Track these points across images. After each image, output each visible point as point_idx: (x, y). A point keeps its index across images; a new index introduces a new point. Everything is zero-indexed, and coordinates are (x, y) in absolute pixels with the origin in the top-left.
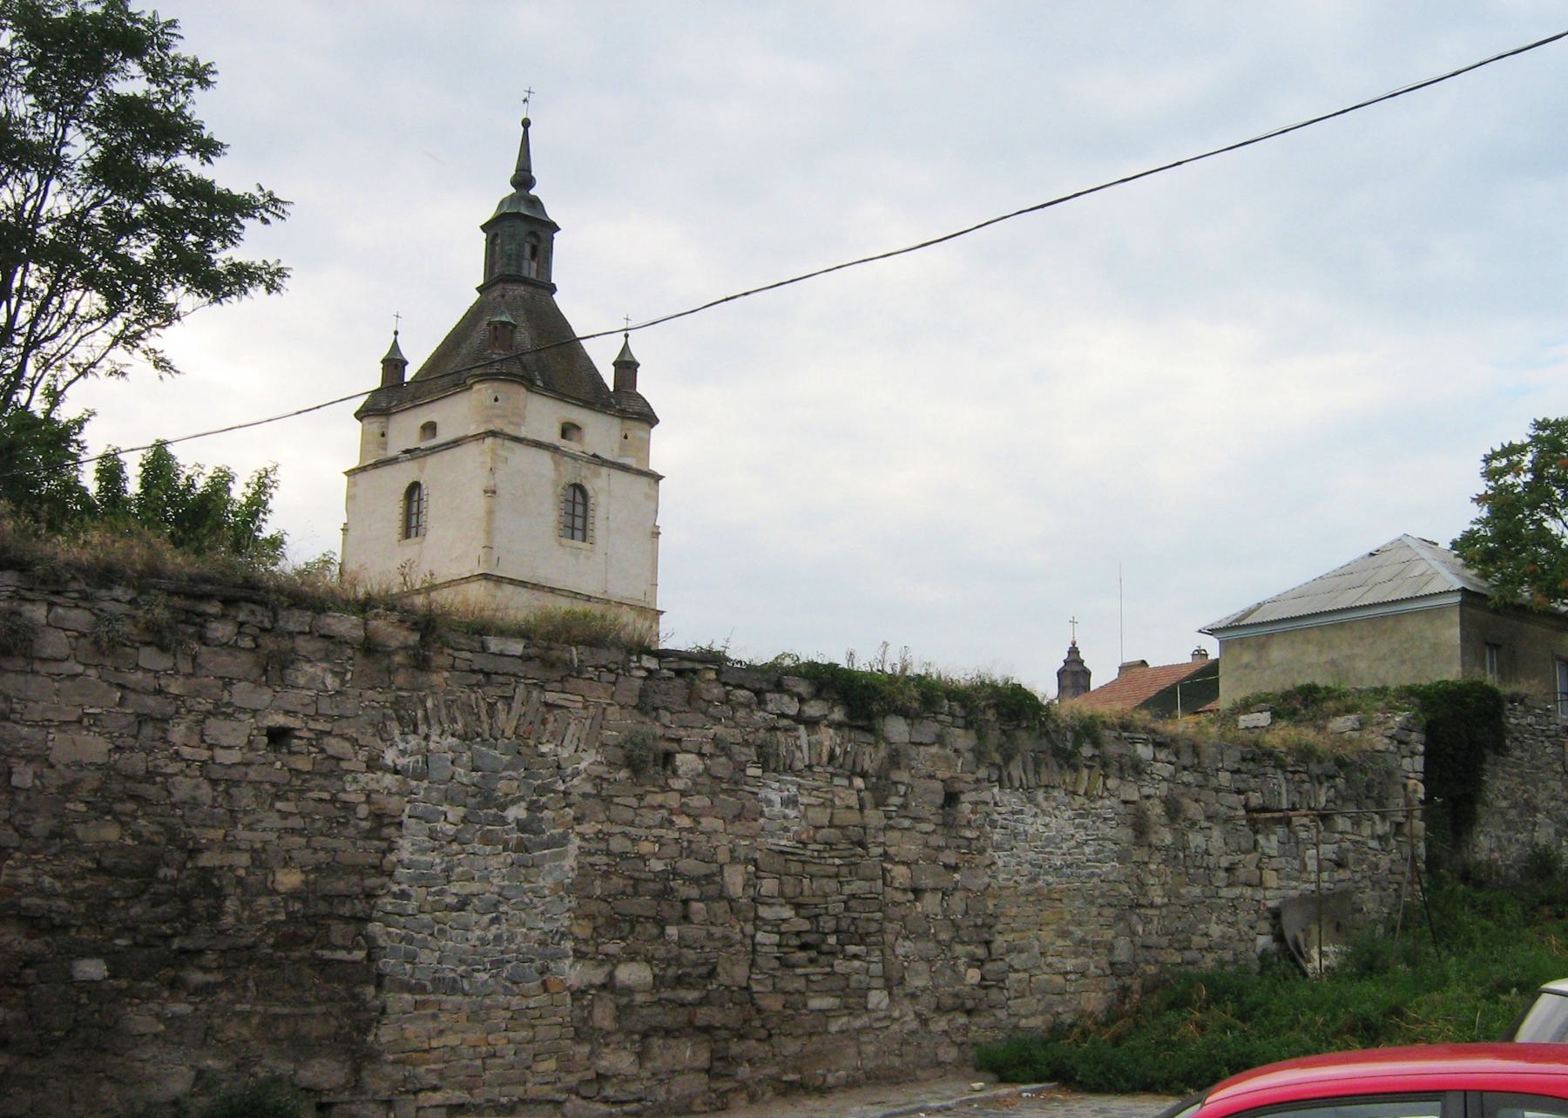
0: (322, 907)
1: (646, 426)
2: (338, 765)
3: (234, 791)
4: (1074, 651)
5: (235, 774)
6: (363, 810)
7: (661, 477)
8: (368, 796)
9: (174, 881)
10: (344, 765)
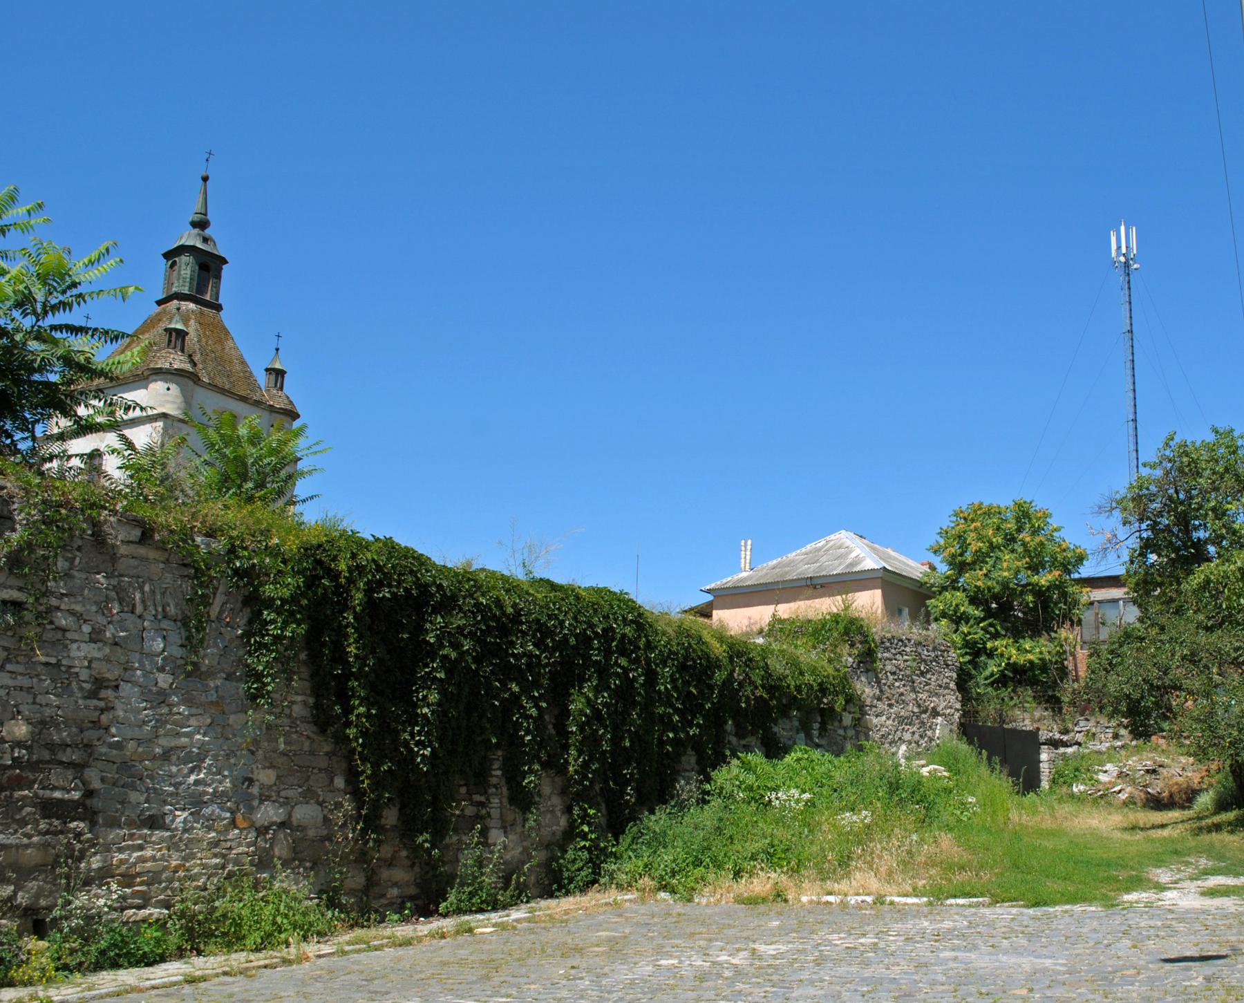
0: (46, 755)
1: (289, 419)
2: (64, 635)
6: (84, 675)
8: (90, 662)
10: (68, 635)
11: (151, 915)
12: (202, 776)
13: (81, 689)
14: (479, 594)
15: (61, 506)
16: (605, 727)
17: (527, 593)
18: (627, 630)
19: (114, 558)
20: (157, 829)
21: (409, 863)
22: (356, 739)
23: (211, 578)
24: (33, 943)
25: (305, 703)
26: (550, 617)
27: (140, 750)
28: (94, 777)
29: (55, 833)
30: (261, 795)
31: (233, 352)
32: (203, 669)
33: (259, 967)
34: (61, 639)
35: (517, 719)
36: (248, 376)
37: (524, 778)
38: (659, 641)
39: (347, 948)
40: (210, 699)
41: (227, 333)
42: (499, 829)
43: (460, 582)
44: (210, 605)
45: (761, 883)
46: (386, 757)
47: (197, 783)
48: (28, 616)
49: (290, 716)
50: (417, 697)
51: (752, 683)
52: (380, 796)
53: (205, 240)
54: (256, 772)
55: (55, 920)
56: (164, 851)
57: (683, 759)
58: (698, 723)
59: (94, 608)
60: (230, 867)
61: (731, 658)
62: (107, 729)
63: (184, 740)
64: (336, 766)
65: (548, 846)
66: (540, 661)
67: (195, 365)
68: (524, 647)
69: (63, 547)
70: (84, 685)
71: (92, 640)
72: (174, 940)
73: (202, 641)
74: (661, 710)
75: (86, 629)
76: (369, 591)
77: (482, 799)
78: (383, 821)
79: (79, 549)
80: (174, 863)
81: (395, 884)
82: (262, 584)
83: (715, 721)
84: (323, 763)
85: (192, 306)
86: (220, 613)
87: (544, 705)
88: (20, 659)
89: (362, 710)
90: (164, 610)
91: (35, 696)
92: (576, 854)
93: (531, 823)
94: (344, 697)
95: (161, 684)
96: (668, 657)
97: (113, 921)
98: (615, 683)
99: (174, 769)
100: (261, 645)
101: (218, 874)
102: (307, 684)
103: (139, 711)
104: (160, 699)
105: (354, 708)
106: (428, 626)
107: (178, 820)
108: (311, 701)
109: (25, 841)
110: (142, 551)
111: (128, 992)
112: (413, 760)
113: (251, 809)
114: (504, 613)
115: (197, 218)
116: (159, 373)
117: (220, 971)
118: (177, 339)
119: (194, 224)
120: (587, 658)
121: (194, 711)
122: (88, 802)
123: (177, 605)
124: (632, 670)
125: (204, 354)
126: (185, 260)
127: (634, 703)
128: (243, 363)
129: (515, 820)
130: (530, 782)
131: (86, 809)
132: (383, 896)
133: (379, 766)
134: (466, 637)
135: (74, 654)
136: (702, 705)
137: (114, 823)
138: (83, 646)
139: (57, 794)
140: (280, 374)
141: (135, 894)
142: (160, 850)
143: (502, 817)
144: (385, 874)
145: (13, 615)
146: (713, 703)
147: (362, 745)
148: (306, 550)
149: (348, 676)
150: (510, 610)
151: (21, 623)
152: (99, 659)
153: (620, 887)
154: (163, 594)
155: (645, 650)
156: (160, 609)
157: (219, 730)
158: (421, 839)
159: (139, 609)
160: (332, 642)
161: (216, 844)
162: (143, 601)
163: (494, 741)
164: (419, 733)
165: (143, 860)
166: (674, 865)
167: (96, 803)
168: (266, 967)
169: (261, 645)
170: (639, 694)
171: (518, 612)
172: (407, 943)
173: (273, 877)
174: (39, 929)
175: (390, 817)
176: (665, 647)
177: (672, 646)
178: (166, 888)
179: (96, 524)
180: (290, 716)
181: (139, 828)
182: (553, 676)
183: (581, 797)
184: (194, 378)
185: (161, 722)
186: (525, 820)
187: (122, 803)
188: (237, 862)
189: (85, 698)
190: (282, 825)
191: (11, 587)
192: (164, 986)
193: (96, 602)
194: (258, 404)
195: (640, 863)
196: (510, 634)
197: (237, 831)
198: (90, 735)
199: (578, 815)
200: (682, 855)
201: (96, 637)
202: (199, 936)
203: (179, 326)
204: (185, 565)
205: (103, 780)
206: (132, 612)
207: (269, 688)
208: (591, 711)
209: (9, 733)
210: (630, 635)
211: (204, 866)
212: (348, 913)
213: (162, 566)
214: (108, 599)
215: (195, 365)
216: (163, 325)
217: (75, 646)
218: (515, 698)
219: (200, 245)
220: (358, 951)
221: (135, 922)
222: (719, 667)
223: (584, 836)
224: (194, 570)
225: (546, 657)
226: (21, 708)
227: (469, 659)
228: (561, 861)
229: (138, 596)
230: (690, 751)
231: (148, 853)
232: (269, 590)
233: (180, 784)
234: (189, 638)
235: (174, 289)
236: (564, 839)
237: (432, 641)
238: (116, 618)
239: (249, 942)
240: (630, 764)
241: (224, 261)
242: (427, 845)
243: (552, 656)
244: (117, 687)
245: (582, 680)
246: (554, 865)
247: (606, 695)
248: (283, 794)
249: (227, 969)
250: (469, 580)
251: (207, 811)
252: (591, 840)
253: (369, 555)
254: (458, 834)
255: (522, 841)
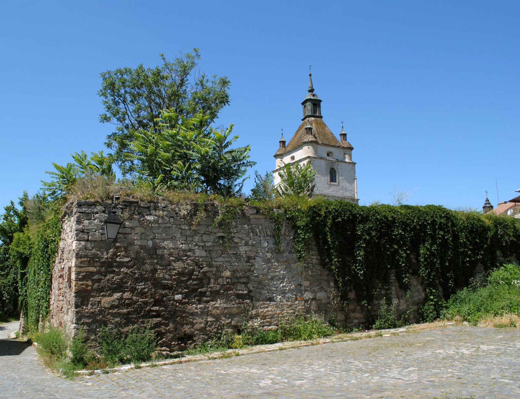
0: (236, 280)
1: (350, 150)
3: (211, 252)
4: (487, 200)
5: (211, 248)
6: (244, 256)
7: (356, 163)
8: (246, 252)
9: (198, 275)
10: (239, 244)
11: (272, 328)
12: (284, 284)
13: (244, 260)
14: (377, 214)
15: (231, 207)
16: (437, 258)
17: (398, 212)
18: (442, 220)
19: (249, 220)
20: (272, 301)
21: (361, 311)
22: (335, 270)
23: (280, 222)
24: (237, 336)
25: (317, 259)
26: (408, 219)
27: (264, 277)
28: (250, 286)
29: (241, 304)
30: (305, 290)
31: (328, 131)
32: (281, 250)
33: (304, 346)
34: (236, 246)
35: (398, 258)
36: (334, 138)
37: (404, 279)
38: (459, 223)
39: (334, 340)
40: (284, 260)
41: (325, 125)
42: (396, 298)
43: (369, 211)
44: (280, 230)
45: (505, 319)
46: (347, 275)
47: (283, 286)
48: (226, 240)
49: (312, 263)
50: (356, 254)
51: (508, 235)
52: (346, 288)
53: (314, 95)
54: (302, 282)
55: (243, 329)
56: (275, 308)
57: (477, 268)
58: (481, 253)
59: (245, 235)
60: (297, 313)
61: (496, 226)
62: (253, 272)
63: (277, 273)
64: (330, 279)
65: (418, 304)
66: (405, 236)
67: (316, 138)
68: (398, 232)
69: (233, 218)
70: (245, 259)
71: (245, 245)
72: (279, 336)
73: (279, 242)
74: (462, 250)
75: (243, 242)
76: (334, 219)
77: (387, 287)
78: (349, 297)
79: (239, 218)
80: (278, 312)
81: (356, 318)
82: (297, 221)
83: (491, 252)
84: (326, 278)
85: (313, 119)
86: (285, 232)
87: (409, 252)
88: (225, 253)
89: (336, 259)
90: (266, 233)
91: (231, 263)
92: (429, 307)
93: (408, 296)
94: (329, 256)
95: (268, 256)
96: (464, 228)
97: (260, 330)
98: (439, 241)
99: (275, 283)
100: (299, 241)
101: (292, 315)
102: (317, 252)
103: (262, 265)
104: (268, 261)
105: (333, 259)
106: (357, 228)
107: (278, 299)
108: (319, 258)
109: (233, 306)
110: (257, 216)
111: (261, 352)
112: (357, 276)
113: (302, 294)
114: (388, 220)
115: (310, 89)
116: (305, 143)
117: (290, 346)
118: (309, 131)
119: (309, 91)
120: (425, 233)
121: (280, 264)
122: (250, 294)
123: (270, 231)
124: (446, 235)
125: (319, 134)
126: (308, 104)
127: (449, 248)
128: (332, 134)
129: (402, 295)
130: (406, 281)
131: (249, 296)
132: (352, 322)
133: (344, 278)
134: (373, 231)
135: (241, 250)
136: (483, 246)
137: (258, 300)
138: (243, 247)
139: (240, 292)
140: (344, 135)
141: (267, 322)
142: (273, 308)
143: (397, 294)
144: (352, 315)
145: (222, 240)
146: (488, 245)
147: (338, 272)
148: (310, 208)
149: (329, 248)
150: (390, 219)
151: (224, 242)
152: (248, 251)
153: (448, 320)
154: (266, 229)
155: (451, 227)
156: (265, 233)
157: (289, 269)
158: (363, 303)
159: (259, 234)
160: (323, 238)
161: (291, 306)
162: (260, 232)
163: (389, 267)
164: (359, 266)
165: (268, 311)
166: (469, 311)
167: (252, 294)
168: (306, 346)
169: (299, 241)
170: (450, 244)
171: (394, 219)
172: (357, 339)
173: (311, 316)
174: (239, 332)
175: (352, 295)
176: (462, 224)
177: (465, 224)
178: (276, 320)
179: (242, 211)
180: (312, 263)
181: (266, 301)
182: (412, 241)
183: (429, 285)
184: (316, 143)
185: (269, 268)
186: (406, 294)
187: (260, 294)
188: (299, 312)
189: (245, 263)
190: (313, 299)
191: (220, 232)
192: (273, 351)
193: (245, 234)
194: (339, 147)
195: (455, 310)
196: (392, 227)
197: (298, 302)
198: (248, 274)
199: (428, 292)
200: (472, 307)
201: (246, 244)
202: (287, 335)
203: (309, 126)
204: (271, 219)
205: (253, 287)
206: (257, 235)
207: (303, 255)
208: (429, 253)
209: (225, 275)
210: (444, 222)
211: (287, 313)
212: (338, 328)
213: (264, 220)
214: (249, 232)
215: (316, 138)
216: (305, 127)
217: (241, 247)
218: (396, 251)
219: (312, 98)
220: (338, 342)
221: (267, 330)
222: (490, 230)
223: (432, 300)
224: (275, 220)
225: (407, 234)
226: (227, 267)
227: (375, 239)
228: (423, 310)
229: (258, 230)
230: (479, 264)
231: (270, 309)
232: (299, 223)
233: (278, 287)
234: (275, 241)
235: (307, 114)
236: (424, 301)
237: (359, 233)
238: (252, 238)
239: (304, 336)
240: (450, 272)
241: (320, 101)
242: (366, 305)
243: (410, 233)
244: (255, 259)
245: (424, 242)
246: (420, 311)
247: (435, 246)
248: (312, 289)
249: (293, 346)
250: (373, 210)
251: (287, 296)
252: (435, 302)
253: (332, 207)
254: (378, 301)
255: (406, 302)
